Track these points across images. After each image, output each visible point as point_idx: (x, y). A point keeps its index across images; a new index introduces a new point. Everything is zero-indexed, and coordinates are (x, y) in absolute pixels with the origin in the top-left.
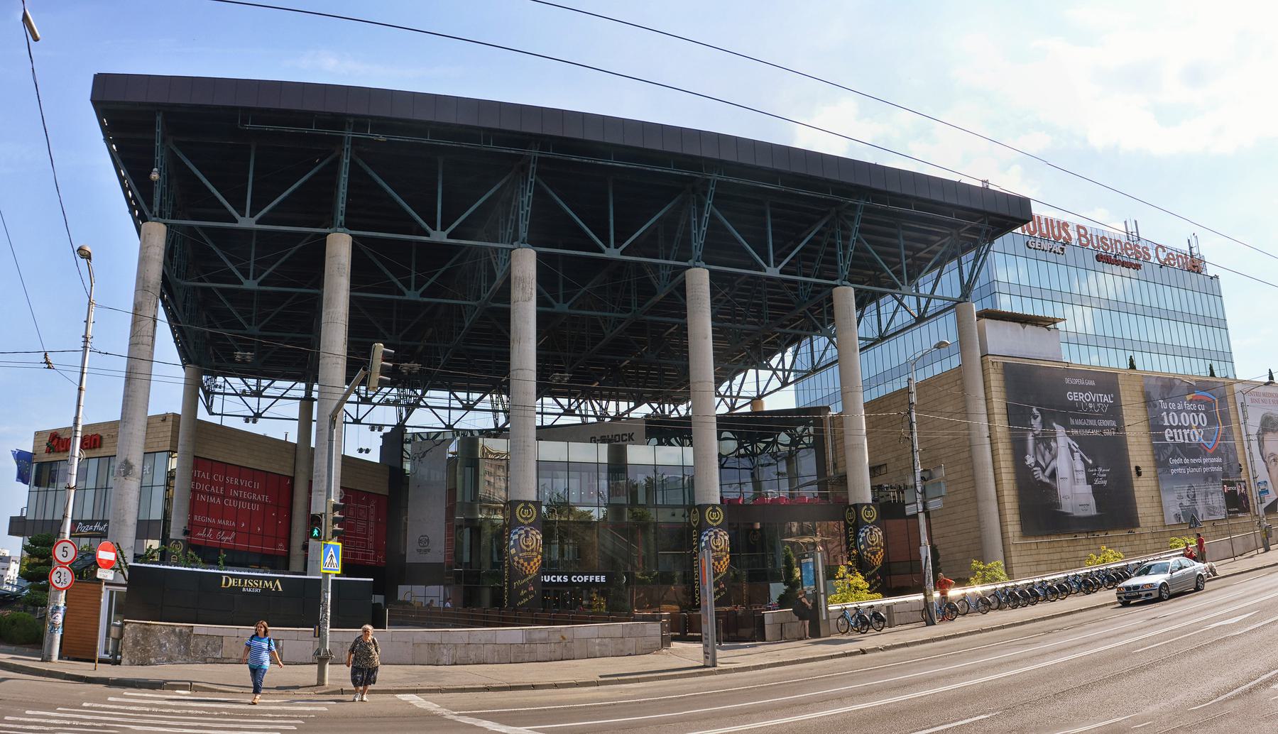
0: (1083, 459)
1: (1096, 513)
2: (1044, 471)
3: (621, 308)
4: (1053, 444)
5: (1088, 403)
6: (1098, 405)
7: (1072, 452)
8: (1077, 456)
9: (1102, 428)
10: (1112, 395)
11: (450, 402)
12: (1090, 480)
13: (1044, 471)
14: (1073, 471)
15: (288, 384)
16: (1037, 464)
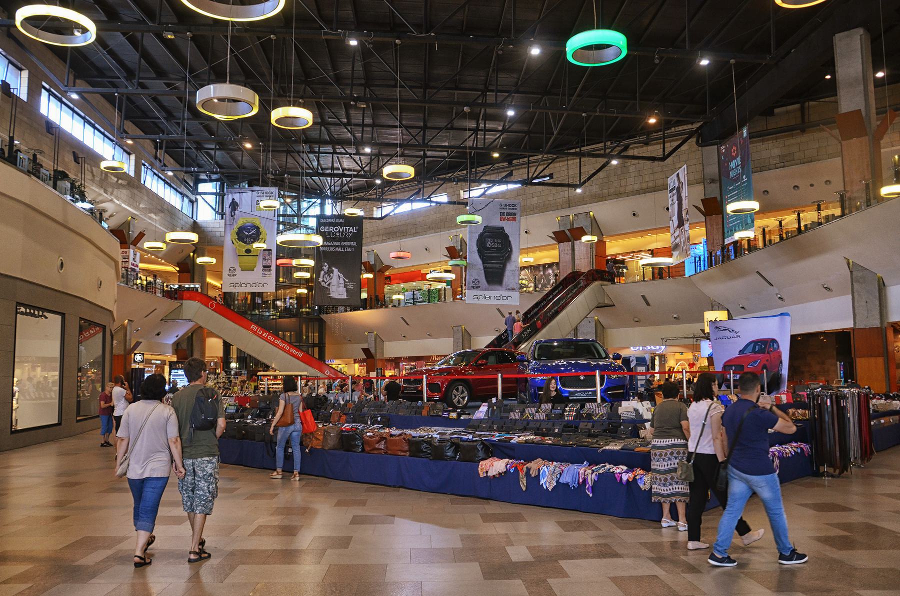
0: (344, 280)
1: (346, 297)
2: (326, 283)
3: (79, 193)
4: (331, 275)
5: (336, 232)
6: (344, 233)
7: (339, 277)
8: (341, 279)
9: (344, 247)
10: (357, 227)
11: (485, 136)
12: (345, 286)
13: (326, 283)
14: (338, 283)
15: (316, 200)
16: (323, 281)
